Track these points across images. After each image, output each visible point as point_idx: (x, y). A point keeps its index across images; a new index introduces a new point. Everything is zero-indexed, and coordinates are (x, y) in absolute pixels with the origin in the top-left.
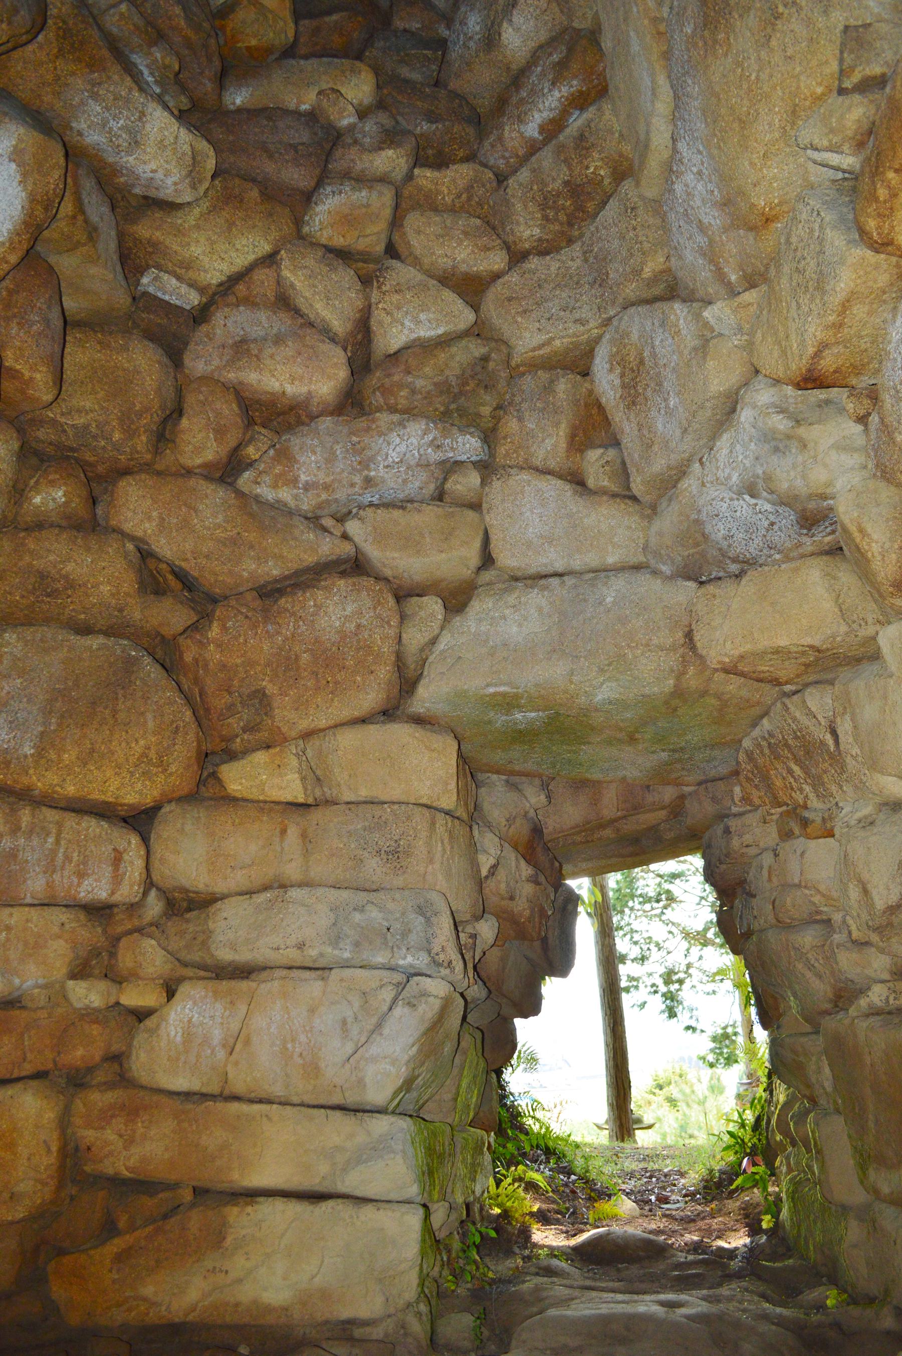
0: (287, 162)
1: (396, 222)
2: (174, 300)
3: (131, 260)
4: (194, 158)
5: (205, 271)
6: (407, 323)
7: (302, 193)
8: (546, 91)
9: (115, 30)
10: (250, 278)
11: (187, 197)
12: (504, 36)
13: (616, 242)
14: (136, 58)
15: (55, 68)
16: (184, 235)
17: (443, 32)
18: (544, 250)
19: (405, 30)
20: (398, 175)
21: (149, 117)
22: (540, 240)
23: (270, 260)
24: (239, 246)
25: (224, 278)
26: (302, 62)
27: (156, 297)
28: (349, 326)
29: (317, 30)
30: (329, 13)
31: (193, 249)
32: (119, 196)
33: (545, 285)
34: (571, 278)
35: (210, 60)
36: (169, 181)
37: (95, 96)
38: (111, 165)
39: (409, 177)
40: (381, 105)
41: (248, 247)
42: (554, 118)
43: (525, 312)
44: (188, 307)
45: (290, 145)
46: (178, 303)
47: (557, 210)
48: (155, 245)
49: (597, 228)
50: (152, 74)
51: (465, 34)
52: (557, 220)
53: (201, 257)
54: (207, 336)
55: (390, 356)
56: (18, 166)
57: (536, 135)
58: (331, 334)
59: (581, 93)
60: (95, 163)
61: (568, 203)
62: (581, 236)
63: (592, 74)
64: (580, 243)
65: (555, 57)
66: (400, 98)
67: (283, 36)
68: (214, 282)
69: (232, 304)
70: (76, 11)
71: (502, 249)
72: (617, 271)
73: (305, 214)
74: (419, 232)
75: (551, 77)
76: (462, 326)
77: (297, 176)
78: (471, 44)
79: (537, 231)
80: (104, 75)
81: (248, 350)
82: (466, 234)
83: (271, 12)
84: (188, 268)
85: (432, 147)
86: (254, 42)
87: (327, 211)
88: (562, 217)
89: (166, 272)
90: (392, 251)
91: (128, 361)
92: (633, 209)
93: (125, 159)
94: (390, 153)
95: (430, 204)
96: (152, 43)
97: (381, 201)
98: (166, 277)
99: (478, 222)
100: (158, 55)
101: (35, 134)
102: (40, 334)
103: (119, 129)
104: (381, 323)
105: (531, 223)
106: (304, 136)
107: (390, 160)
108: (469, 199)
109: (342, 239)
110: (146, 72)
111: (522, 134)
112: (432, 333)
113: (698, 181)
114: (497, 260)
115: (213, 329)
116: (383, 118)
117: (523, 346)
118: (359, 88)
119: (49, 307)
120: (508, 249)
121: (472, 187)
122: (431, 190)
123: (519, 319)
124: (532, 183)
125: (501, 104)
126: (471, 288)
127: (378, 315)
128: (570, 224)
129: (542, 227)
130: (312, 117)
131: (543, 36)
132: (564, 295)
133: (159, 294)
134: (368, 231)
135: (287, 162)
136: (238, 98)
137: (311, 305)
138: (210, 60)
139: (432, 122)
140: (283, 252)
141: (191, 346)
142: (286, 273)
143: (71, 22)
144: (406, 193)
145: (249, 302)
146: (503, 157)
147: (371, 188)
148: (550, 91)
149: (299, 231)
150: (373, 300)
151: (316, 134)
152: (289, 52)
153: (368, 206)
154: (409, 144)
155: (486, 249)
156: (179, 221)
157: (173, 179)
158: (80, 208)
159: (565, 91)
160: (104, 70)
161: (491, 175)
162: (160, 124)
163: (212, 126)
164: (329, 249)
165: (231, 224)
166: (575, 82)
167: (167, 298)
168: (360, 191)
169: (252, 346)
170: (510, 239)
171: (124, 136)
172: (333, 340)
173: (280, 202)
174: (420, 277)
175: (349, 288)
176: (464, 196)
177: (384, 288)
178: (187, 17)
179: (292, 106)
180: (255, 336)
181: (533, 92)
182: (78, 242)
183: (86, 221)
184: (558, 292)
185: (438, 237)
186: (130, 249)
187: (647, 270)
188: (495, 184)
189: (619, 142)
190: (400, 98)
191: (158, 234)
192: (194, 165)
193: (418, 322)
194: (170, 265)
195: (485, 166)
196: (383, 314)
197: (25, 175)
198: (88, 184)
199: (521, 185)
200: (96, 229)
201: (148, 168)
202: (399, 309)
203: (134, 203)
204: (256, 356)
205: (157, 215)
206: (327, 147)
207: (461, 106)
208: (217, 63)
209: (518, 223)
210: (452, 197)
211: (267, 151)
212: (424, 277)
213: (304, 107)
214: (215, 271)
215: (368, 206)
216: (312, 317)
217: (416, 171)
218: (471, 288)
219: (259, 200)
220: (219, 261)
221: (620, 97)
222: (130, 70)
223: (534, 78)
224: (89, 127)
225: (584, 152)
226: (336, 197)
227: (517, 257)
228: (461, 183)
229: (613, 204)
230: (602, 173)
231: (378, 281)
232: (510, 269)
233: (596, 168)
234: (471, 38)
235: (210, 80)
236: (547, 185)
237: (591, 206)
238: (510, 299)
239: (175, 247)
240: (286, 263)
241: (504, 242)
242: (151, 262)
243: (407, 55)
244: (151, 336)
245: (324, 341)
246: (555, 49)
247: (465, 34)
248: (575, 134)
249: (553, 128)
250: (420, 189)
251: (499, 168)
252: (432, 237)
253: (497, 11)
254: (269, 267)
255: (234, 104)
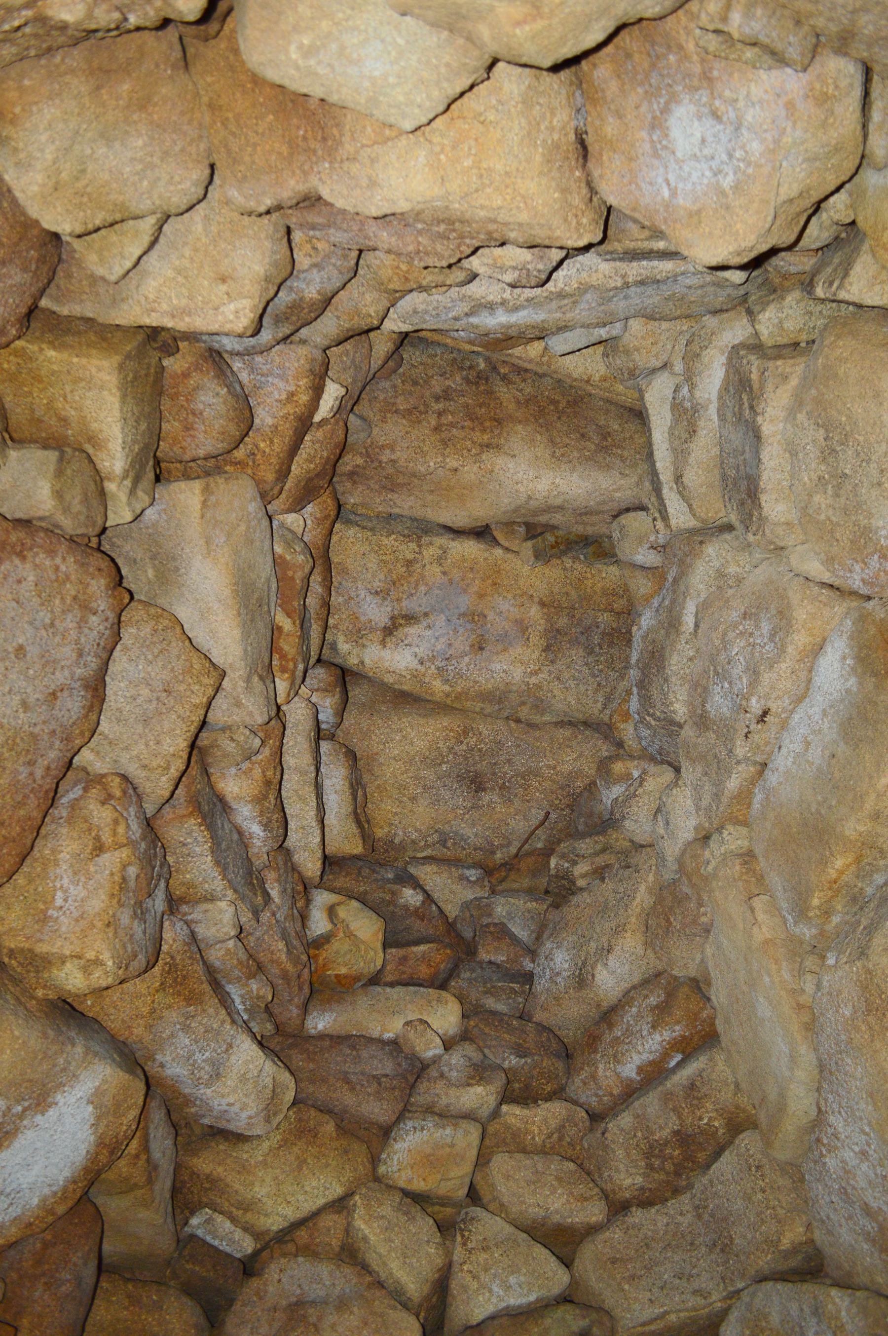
0: (369, 1095)
1: (482, 1160)
2: (224, 1247)
3: (185, 1197)
4: (274, 1091)
5: (266, 1215)
6: (495, 1289)
7: (380, 1127)
8: (645, 1033)
9: (217, 964)
10: (314, 1224)
11: (258, 1131)
12: (598, 977)
13: (739, 1202)
14: (230, 988)
15: (153, 1002)
16: (249, 1172)
17: (528, 965)
18: (647, 1200)
19: (490, 962)
20: (485, 1112)
21: (235, 1049)
22: (642, 1189)
23: (341, 1205)
24: (307, 1189)
25: (286, 1224)
26: (388, 990)
27: (204, 1242)
28: (426, 1289)
29: (404, 960)
30: (417, 943)
31: (257, 1189)
32: (183, 1123)
33: (653, 1244)
34: (683, 1236)
35: (300, 989)
36: (244, 1115)
37: (186, 1028)
38: (184, 1096)
39: (496, 1114)
40: (465, 1036)
41: (319, 1187)
42: (653, 1061)
43: (633, 1277)
44: (238, 1256)
45: (374, 1077)
46: (228, 1249)
47: (664, 1158)
48: (213, 1181)
49: (711, 1182)
50: (244, 1003)
51: (552, 969)
52: (663, 1169)
53: (264, 1200)
54: (257, 1294)
55: (472, 1327)
56: (95, 1108)
57: (633, 1075)
58: (403, 1298)
59: (684, 1037)
60: (169, 1093)
61: (677, 1152)
62: (690, 1186)
63: (696, 1020)
64: (688, 1195)
65: (653, 1000)
66: (487, 1030)
67: (372, 965)
68: (275, 1228)
69: (290, 1254)
70: (186, 948)
71: (600, 1199)
72: (745, 1237)
73: (382, 1151)
74: (508, 1177)
75: (650, 1019)
76: (556, 1291)
77: (377, 1110)
78: (559, 979)
79: (639, 1180)
80: (199, 1008)
81: (304, 1316)
82: (559, 1179)
83: (363, 942)
84: (246, 1210)
85: (519, 1081)
86: (343, 971)
87: (409, 1152)
88: (669, 1166)
89: (221, 1213)
90: (473, 1196)
91: (160, 1325)
92: (758, 1167)
93: (202, 1091)
94: (479, 1089)
95: (519, 1145)
96: (252, 976)
97: (467, 1139)
98: (219, 1218)
99: (572, 1166)
100: (255, 987)
101: (121, 1074)
102: (67, 1296)
103: (204, 1061)
104: (465, 1288)
105: (634, 1171)
106: (385, 1066)
107: (479, 1096)
108: (561, 1139)
109: (422, 1183)
110: (238, 1001)
111: (618, 1075)
112: (524, 1301)
113: (862, 1161)
114: (595, 1212)
115: (265, 1285)
116: (469, 1049)
117: (631, 1319)
118: (446, 1017)
119: (85, 1264)
120: (607, 1197)
121: (564, 1127)
122: (519, 1129)
123: (626, 1287)
124: (635, 1129)
125: (592, 1041)
126: (563, 1242)
127: (461, 1279)
128: (678, 1174)
129: (645, 1176)
130: (395, 1045)
131: (636, 978)
132: (676, 1258)
133: (208, 1238)
134: (452, 1174)
135: (369, 1095)
136: (321, 1022)
137: (385, 1264)
138: (300, 989)
139: (521, 1057)
140: (357, 1198)
141: (237, 1307)
142: (359, 1223)
143: (179, 958)
144: (491, 1129)
145: (310, 1252)
146: (596, 1095)
147: (456, 1125)
148: (650, 1034)
149: (375, 1169)
150: (455, 1258)
151: (399, 1065)
152: (375, 980)
153: (452, 1145)
154: (500, 1081)
155: (584, 1199)
156: (245, 1156)
157: (249, 1113)
158: (145, 1147)
159: (667, 1035)
160: (201, 1003)
161: (584, 1114)
162: (246, 1055)
163: (292, 1052)
164: (406, 1193)
165: (302, 1162)
166: (677, 1028)
167: (216, 1243)
168: (444, 1127)
169: (311, 1311)
170: (608, 1187)
171: (207, 1068)
172: (405, 1306)
173: (358, 1137)
174: (509, 1229)
175: (428, 1242)
176: (555, 1136)
177: (470, 1245)
178: (289, 952)
179: (376, 1034)
180: (313, 1296)
181: (628, 1032)
182: (135, 1185)
183: (148, 1161)
184: (669, 1254)
185: (529, 1183)
186: (184, 1182)
187: (785, 1241)
188: (588, 1124)
189: (736, 1094)
190: (487, 1030)
191: (220, 1169)
192: (272, 1098)
193: (508, 1288)
194: (227, 1204)
195: (575, 1103)
196: (469, 1278)
197: (98, 1118)
198: (157, 1115)
199: (622, 1130)
200: (156, 1168)
201: (224, 1101)
202: (486, 1270)
203: (198, 1131)
204: (315, 1326)
205: (221, 1147)
206: (411, 1079)
207: (549, 1039)
208: (306, 990)
209: (618, 1171)
210: (543, 1137)
211: (348, 1082)
212: (512, 1229)
213: (388, 1036)
214: (276, 1216)
215: (452, 1145)
216: (383, 1276)
217: (504, 1108)
218: (563, 1242)
219: (334, 1135)
220: (284, 1205)
221: (739, 1052)
222: (225, 1001)
223: (628, 1018)
224: (173, 1060)
225: (695, 1102)
226: (418, 1133)
227: (618, 1208)
228: (553, 1123)
229: (727, 1157)
230: (716, 1124)
231: (463, 1236)
232: (609, 1221)
233: (710, 1119)
234: (558, 974)
235: (297, 1007)
236: (653, 1133)
237: (701, 1157)
238: (614, 1261)
239: (237, 1186)
240: (360, 1212)
241: (602, 1190)
242: (205, 1199)
243: (493, 987)
244: (189, 1290)
245: (395, 1308)
246: (651, 992)
247: (552, 969)
248: (685, 1082)
249: (654, 1073)
250: (508, 1127)
251: (590, 1104)
252: (523, 1184)
253: (588, 953)
254: (339, 1212)
255: (316, 1028)
